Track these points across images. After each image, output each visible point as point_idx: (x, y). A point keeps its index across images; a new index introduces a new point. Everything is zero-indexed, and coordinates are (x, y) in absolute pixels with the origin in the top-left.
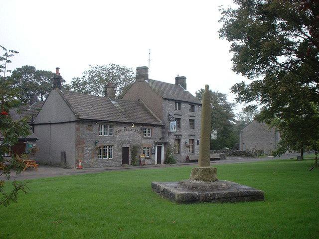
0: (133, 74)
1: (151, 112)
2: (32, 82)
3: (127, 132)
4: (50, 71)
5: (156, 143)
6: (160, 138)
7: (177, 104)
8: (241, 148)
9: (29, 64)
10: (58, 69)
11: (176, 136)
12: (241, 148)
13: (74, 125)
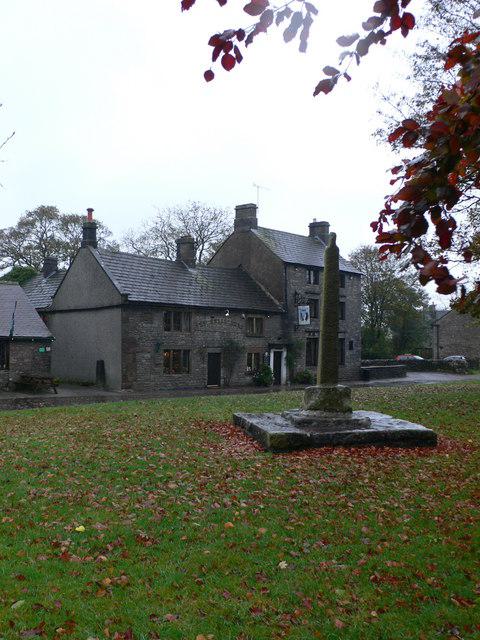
0: (230, 219)
2: (52, 237)
4: (216, 201)
7: (312, 272)
8: (435, 355)
9: (47, 204)
10: (90, 211)
11: (309, 332)
12: (435, 355)
13: (117, 314)
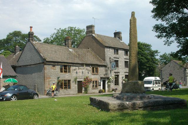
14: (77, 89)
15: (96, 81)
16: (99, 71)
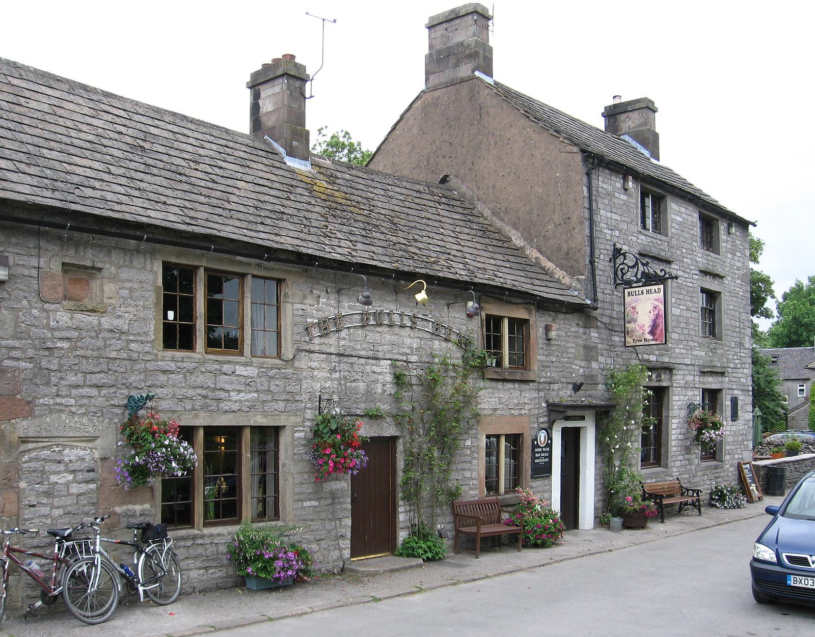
1: (517, 240)
3: (383, 337)
5: (556, 411)
6: (453, 182)
14: (348, 522)
15: (515, 440)
16: (539, 356)
